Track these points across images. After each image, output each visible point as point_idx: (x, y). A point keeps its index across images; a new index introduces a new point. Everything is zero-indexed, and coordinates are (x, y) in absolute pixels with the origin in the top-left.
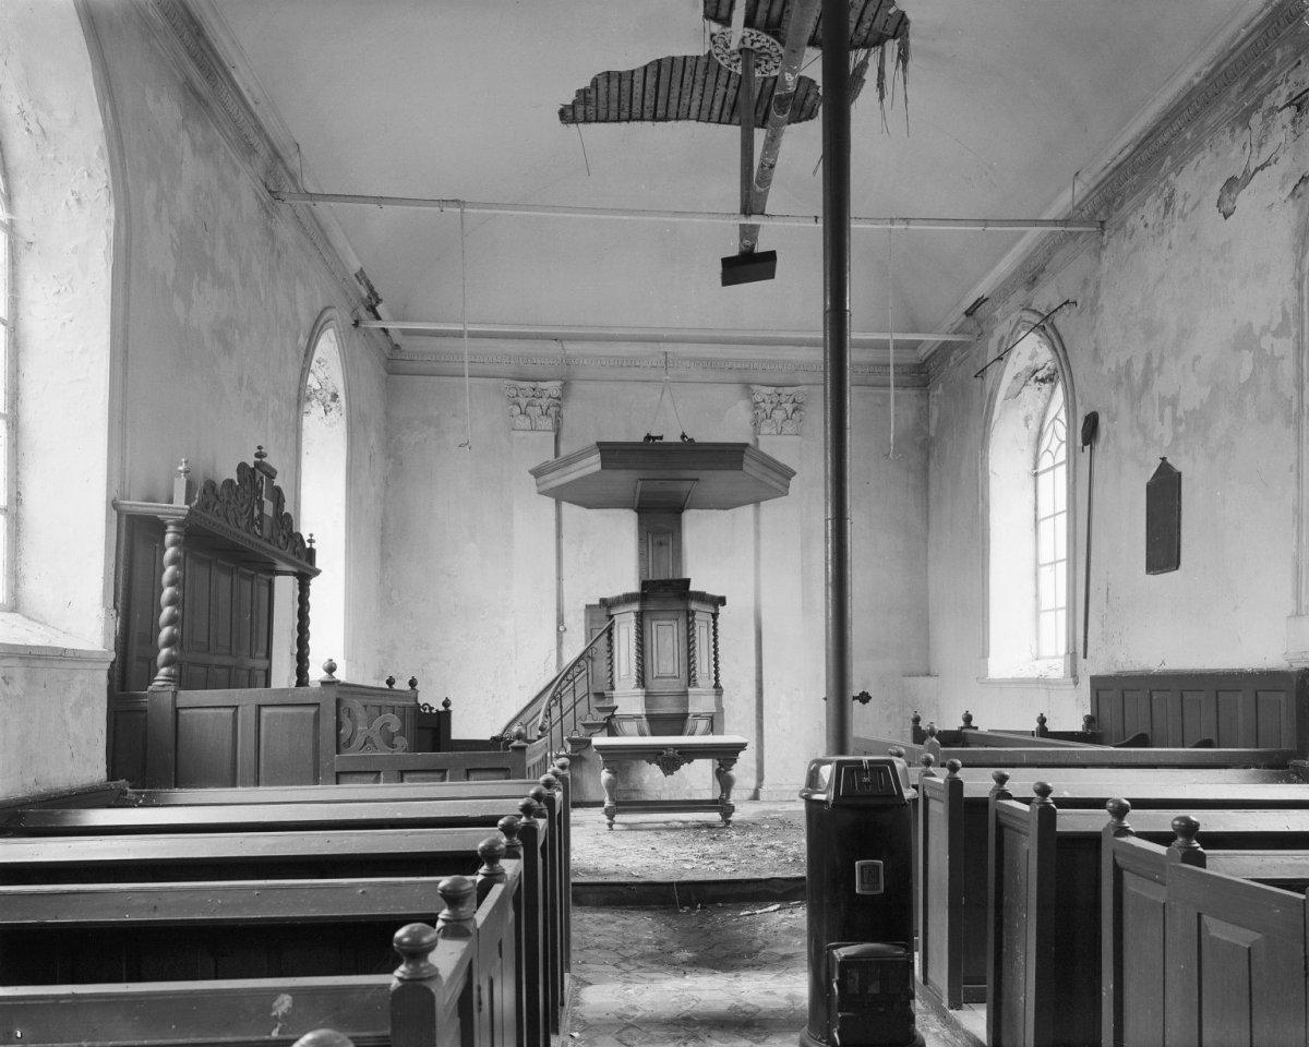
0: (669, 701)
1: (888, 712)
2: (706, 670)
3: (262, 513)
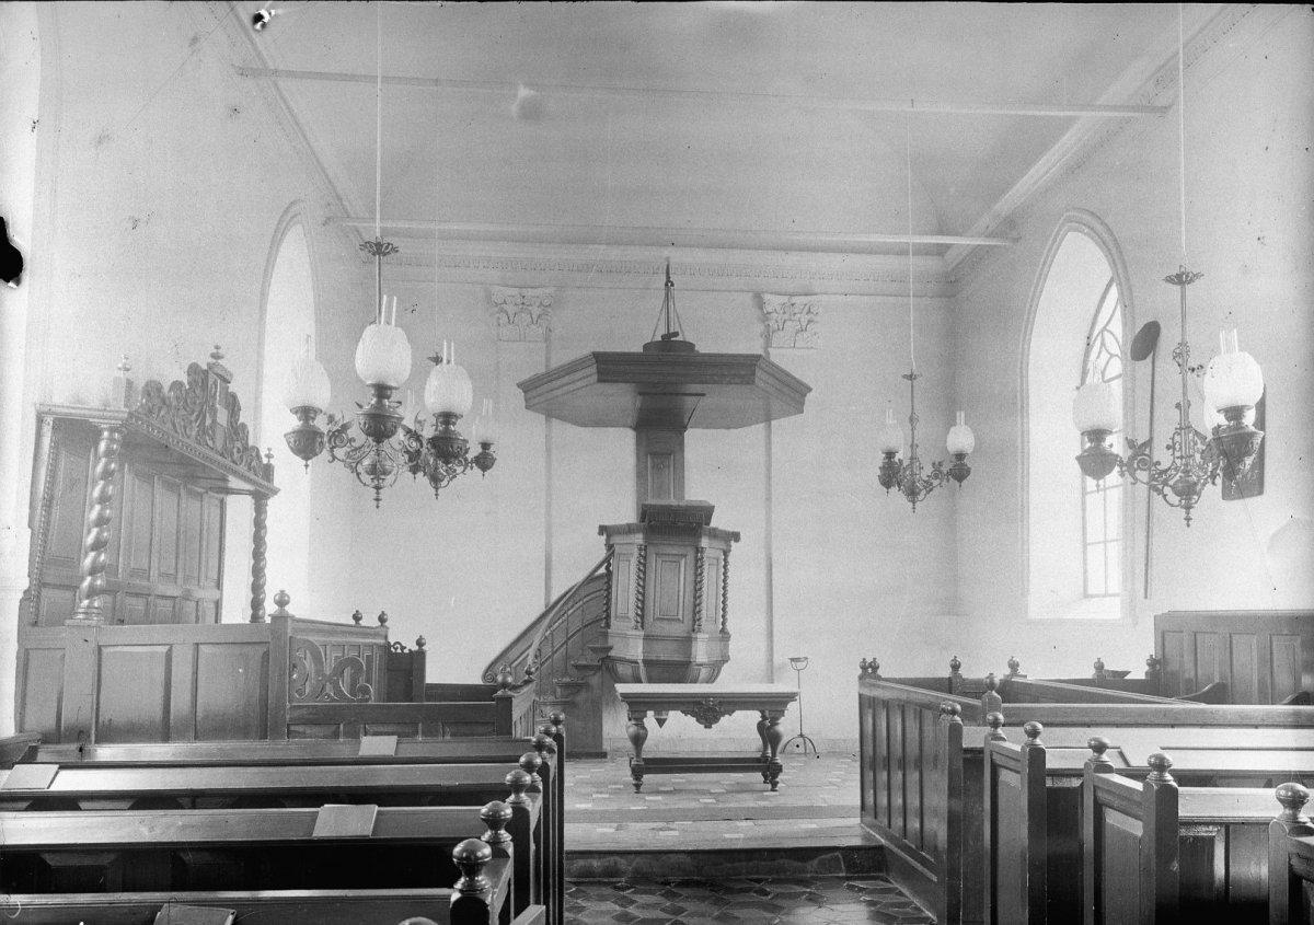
3: (214, 421)
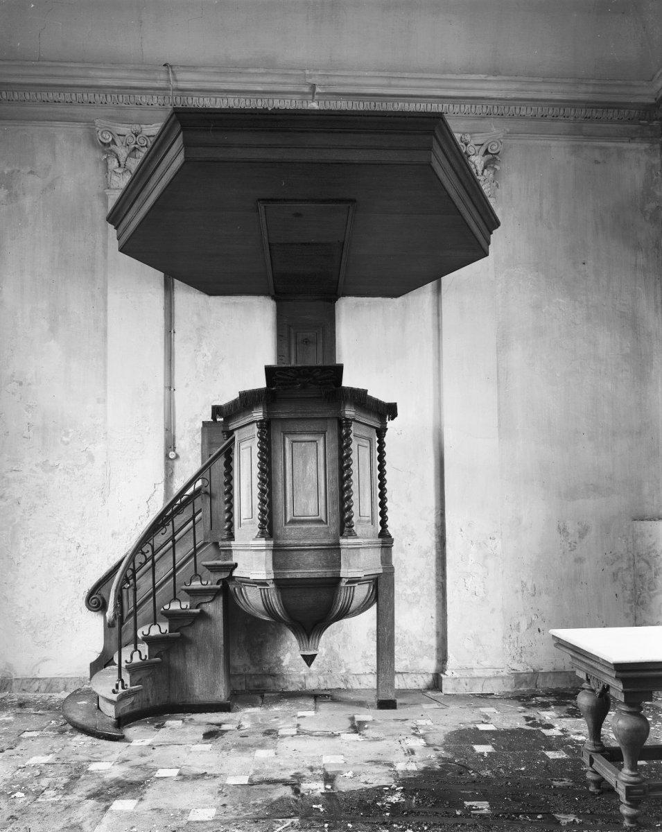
0: (310, 558)
1: (614, 568)
2: (366, 510)
